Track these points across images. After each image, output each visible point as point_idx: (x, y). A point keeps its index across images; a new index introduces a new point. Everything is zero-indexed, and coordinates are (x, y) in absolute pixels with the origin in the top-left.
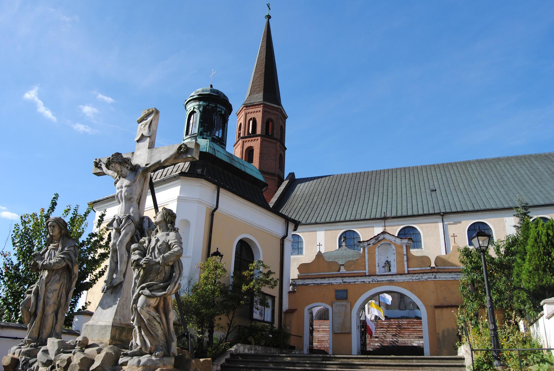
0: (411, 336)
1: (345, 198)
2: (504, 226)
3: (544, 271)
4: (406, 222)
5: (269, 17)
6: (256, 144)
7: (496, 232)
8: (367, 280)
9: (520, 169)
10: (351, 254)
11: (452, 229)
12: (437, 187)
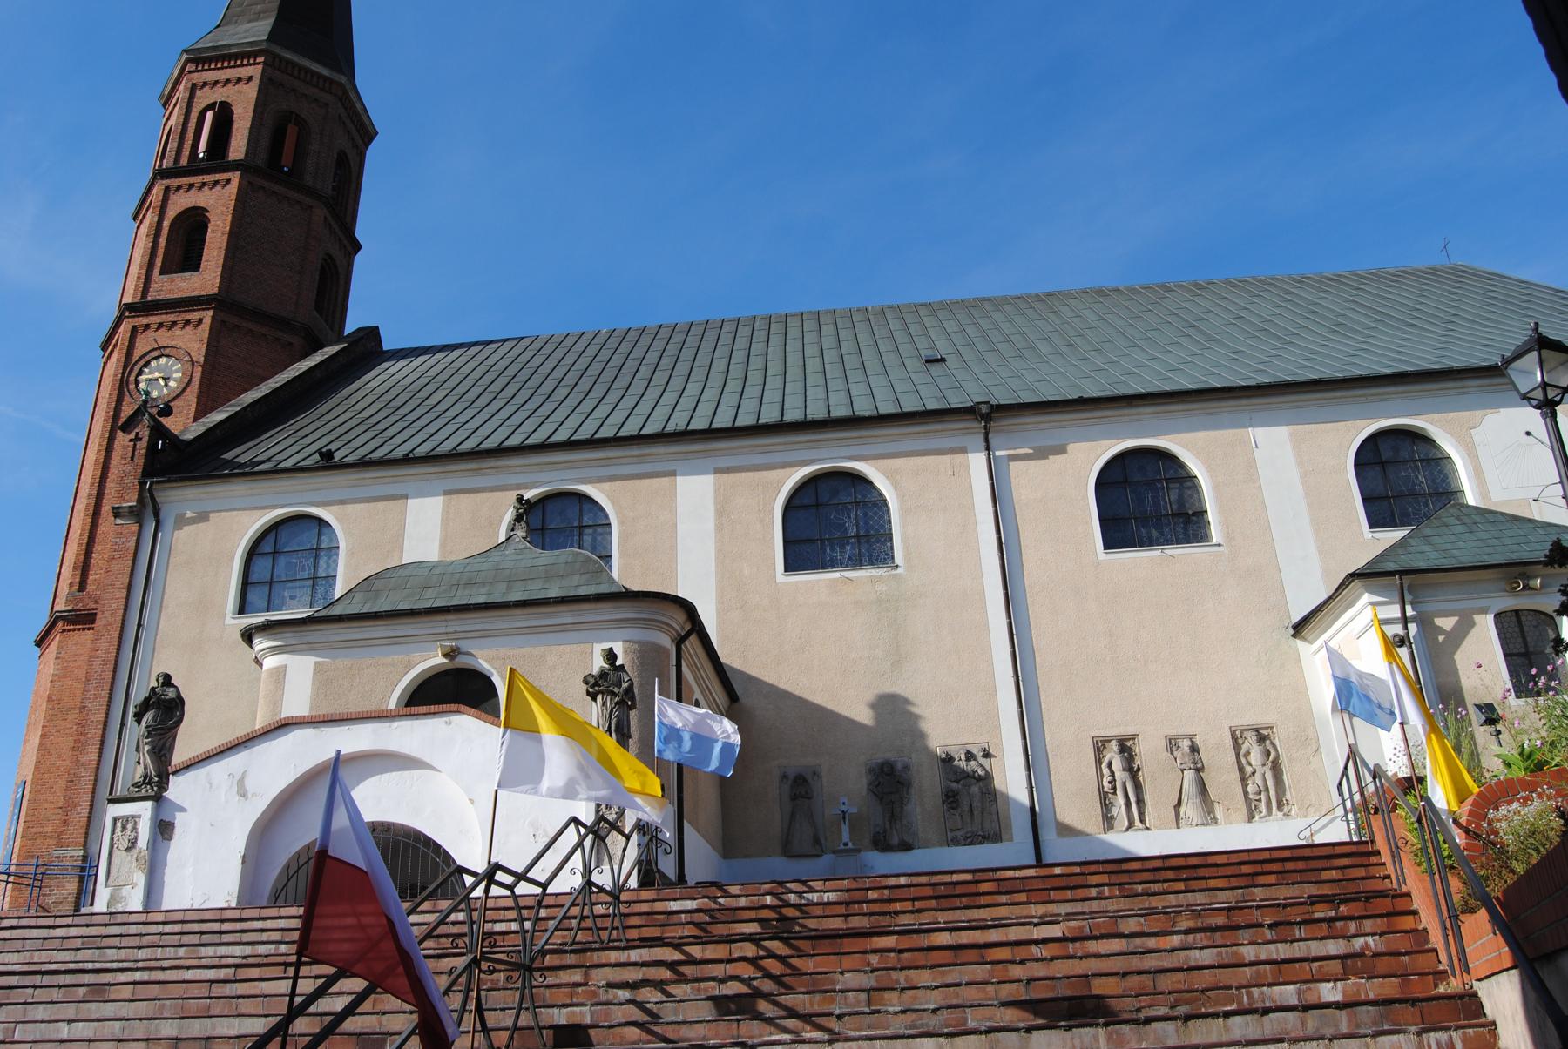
0: (894, 1002)
1: (562, 392)
2: (1251, 464)
4: (824, 453)
6: (218, 201)
7: (1216, 488)
10: (541, 561)
11: (1027, 478)
12: (943, 349)
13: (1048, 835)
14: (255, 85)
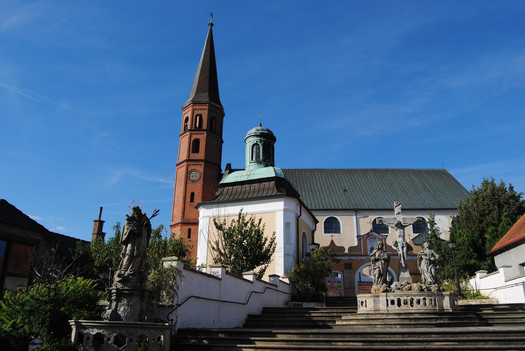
3: (467, 258)
5: (212, 25)
6: (202, 137)
8: (363, 258)
9: (403, 180)
11: (362, 221)
12: (347, 188)
13: (362, 276)
14: (207, 111)
